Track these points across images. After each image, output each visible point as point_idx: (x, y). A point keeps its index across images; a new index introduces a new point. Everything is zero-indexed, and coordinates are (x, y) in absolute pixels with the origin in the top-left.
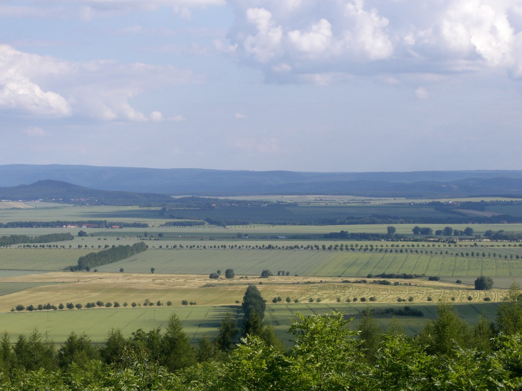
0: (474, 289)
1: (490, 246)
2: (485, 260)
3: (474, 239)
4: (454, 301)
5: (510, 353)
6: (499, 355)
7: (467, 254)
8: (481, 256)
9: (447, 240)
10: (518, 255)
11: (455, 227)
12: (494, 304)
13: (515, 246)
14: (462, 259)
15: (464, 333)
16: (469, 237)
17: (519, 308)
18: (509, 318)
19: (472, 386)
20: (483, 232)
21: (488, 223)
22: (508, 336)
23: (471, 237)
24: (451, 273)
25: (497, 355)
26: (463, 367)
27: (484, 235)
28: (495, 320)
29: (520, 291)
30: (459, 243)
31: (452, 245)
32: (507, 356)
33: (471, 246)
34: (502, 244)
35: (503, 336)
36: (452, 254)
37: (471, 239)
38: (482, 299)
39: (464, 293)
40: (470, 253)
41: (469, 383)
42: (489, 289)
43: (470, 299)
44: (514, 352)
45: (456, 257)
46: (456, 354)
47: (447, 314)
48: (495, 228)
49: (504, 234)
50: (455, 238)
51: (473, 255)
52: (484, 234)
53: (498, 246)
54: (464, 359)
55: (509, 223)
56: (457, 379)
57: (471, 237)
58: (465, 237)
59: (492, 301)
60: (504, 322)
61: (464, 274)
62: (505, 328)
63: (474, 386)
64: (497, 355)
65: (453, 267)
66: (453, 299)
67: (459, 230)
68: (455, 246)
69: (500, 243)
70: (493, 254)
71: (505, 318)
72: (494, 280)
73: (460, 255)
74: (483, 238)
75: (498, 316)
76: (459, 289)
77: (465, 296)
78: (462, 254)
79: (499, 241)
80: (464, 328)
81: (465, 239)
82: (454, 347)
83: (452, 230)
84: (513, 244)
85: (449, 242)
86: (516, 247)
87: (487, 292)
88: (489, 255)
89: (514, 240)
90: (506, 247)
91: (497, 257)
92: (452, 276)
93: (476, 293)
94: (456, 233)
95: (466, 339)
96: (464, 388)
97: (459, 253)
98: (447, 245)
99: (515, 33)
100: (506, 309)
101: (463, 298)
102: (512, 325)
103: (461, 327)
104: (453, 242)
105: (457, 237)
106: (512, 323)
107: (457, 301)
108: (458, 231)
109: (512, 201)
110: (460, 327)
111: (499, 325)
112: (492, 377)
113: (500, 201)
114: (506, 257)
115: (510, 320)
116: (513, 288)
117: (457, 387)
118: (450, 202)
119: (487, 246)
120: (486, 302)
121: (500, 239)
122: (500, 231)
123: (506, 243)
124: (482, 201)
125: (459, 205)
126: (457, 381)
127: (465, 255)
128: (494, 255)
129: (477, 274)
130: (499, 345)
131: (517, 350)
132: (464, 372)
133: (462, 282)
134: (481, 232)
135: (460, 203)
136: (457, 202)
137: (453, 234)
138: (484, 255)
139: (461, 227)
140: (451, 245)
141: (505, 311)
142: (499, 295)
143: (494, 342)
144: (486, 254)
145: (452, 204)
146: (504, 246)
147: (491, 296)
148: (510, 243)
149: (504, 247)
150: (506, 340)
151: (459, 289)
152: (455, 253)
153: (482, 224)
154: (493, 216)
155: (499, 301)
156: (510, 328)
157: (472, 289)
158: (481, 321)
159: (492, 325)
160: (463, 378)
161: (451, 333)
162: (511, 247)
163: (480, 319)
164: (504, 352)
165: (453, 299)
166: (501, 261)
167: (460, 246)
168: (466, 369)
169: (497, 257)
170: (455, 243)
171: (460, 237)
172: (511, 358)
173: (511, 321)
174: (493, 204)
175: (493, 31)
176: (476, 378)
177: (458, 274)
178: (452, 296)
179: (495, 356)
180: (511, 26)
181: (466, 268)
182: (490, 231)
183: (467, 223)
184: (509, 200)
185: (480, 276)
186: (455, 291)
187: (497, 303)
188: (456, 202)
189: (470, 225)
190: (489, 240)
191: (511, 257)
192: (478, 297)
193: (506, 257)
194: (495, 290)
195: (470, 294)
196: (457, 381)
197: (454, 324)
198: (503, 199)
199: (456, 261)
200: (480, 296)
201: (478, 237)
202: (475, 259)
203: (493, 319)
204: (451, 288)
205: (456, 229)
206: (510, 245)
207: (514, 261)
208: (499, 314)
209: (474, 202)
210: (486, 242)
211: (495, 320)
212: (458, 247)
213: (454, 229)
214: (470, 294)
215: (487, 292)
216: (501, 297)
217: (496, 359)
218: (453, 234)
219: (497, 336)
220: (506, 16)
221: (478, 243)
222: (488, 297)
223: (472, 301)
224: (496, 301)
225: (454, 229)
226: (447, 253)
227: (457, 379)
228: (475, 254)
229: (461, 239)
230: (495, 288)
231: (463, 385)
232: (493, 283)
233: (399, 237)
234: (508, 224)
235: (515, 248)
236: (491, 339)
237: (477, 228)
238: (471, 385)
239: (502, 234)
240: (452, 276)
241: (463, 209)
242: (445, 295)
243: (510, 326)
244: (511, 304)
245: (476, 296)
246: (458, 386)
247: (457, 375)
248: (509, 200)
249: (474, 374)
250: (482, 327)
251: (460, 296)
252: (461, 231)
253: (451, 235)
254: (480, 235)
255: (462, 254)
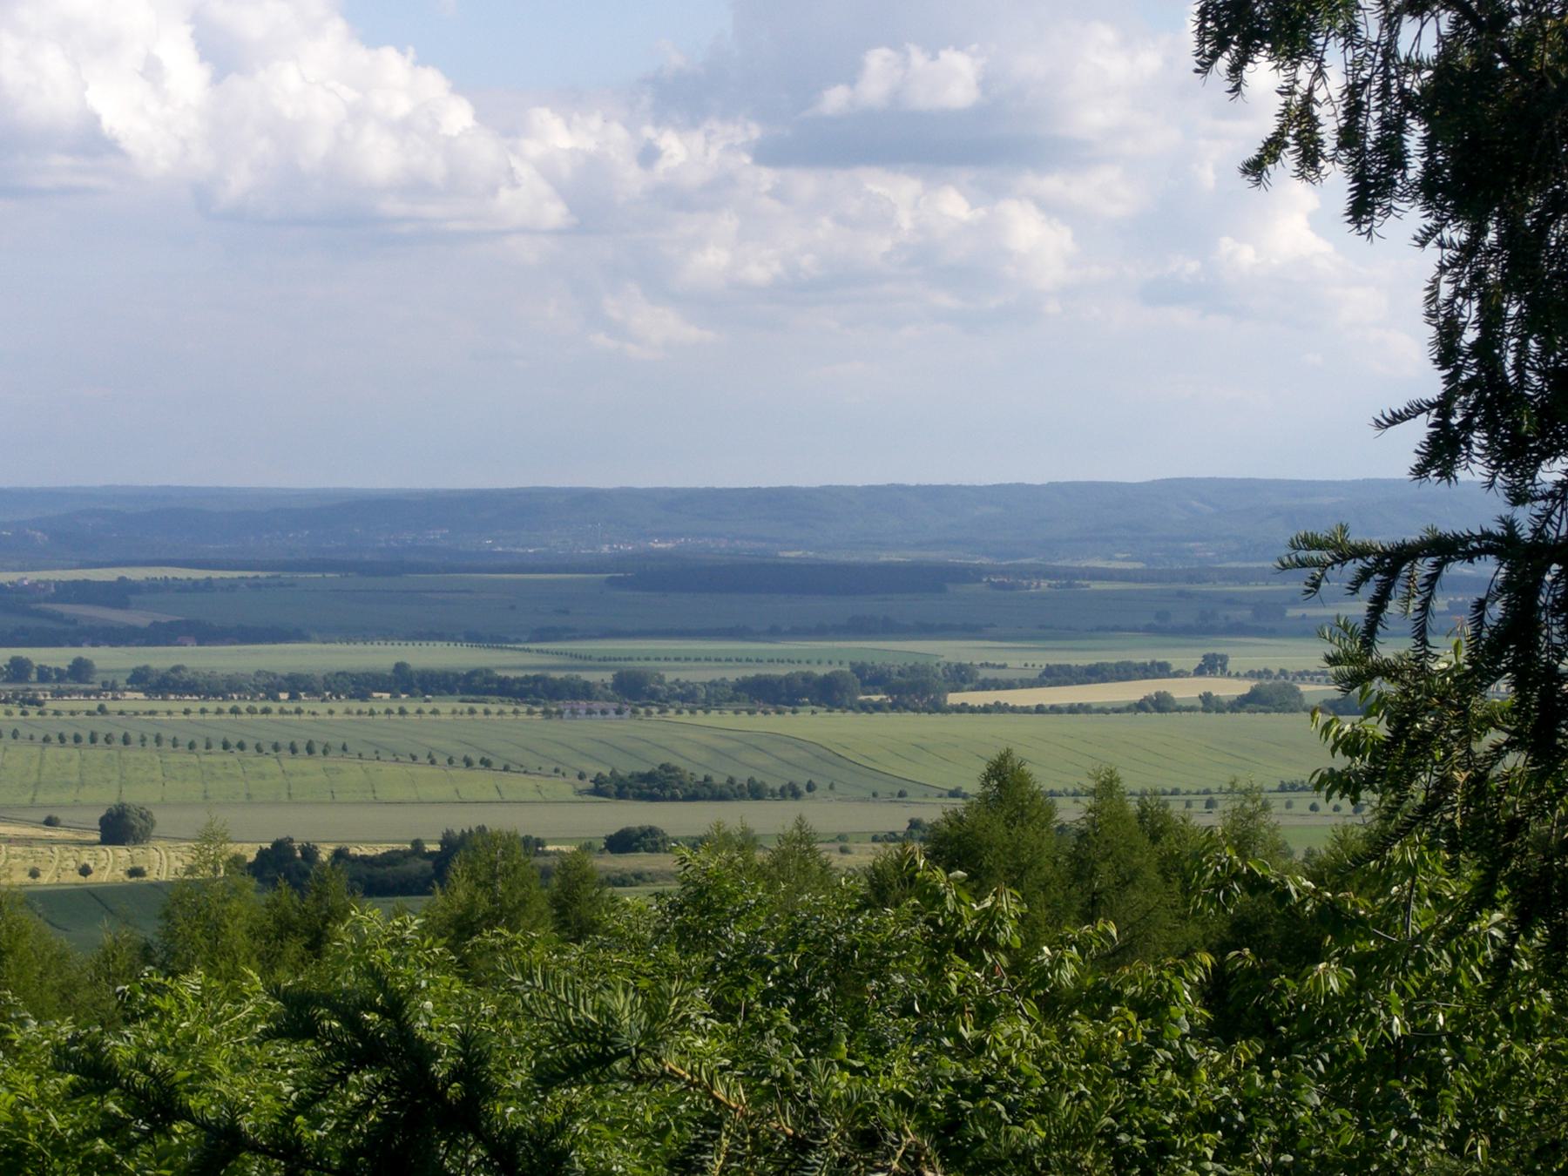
0: (99, 844)
1: (145, 713)
2: (132, 754)
3: (97, 693)
4: (38, 880)
5: (172, 1030)
6: (140, 1035)
7: (77, 739)
8: (118, 744)
9: (15, 697)
10: (229, 740)
11: (40, 656)
12: (157, 886)
13: (219, 712)
14: (63, 753)
15: (60, 973)
16: (82, 686)
17: (226, 896)
18: (196, 927)
19: (56, 1133)
20: (126, 671)
21: (137, 645)
22: (170, 979)
23: (89, 687)
24: (29, 796)
25: (132, 1037)
26: (29, 1073)
27: (129, 682)
28: (155, 933)
29: (229, 845)
30: (51, 705)
31: (33, 712)
32: (162, 1038)
33: (89, 713)
34: (181, 706)
35: (155, 979)
36: (31, 738)
37: (87, 694)
38: (122, 873)
39: (67, 854)
40: (85, 736)
41: (47, 1121)
42: (142, 842)
43: (85, 871)
44: (183, 1025)
45: (43, 748)
46: (11, 1037)
47: (10, 920)
48: (160, 658)
49: (187, 676)
50: (40, 690)
51: (93, 740)
52: (128, 676)
53: (169, 713)
54: (34, 1049)
55: (199, 644)
56: (13, 1111)
57: (89, 687)
58: (72, 686)
59: (152, 876)
60: (181, 938)
61: (68, 797)
62: (184, 956)
63: (62, 1130)
64: (132, 1037)
65: (34, 777)
66: (34, 874)
67: (52, 665)
68: (41, 713)
69: (175, 704)
70: (153, 738)
71: (185, 926)
72: (158, 815)
73: (55, 740)
74: (126, 690)
75: (162, 923)
76: (52, 842)
77: (72, 864)
78: (62, 739)
79: (172, 697)
80: (61, 958)
81: (70, 692)
82: (13, 1015)
83: (32, 666)
84: (212, 705)
85: (24, 702)
86: (223, 717)
87: (137, 851)
88: (143, 740)
89: (216, 695)
90: (192, 717)
91: (167, 746)
92: (33, 805)
93: (103, 855)
94: (44, 675)
95: (65, 991)
96: (31, 1136)
97: (51, 735)
98: (17, 711)
99: (217, 79)
100: (186, 901)
101: (64, 870)
102: (205, 949)
103: (52, 958)
104: (34, 702)
105: (47, 686)
106: (203, 941)
107: (46, 879)
108: (50, 669)
109: (209, 579)
110: (48, 955)
111: (165, 949)
112: (116, 1103)
113: (175, 579)
114: (192, 746)
115: (198, 932)
116: (209, 837)
117: (12, 1136)
118: (26, 583)
119: (136, 713)
120: (134, 880)
121: (175, 693)
122: (176, 669)
123: (193, 703)
124: (122, 579)
125: (53, 590)
126: (10, 1118)
127: (70, 742)
128: (158, 740)
129: (107, 798)
130: (142, 1005)
131: (193, 1019)
132: (32, 1088)
133: (62, 823)
134: (118, 671)
135: (57, 584)
136: (47, 583)
137: (34, 676)
138: (126, 740)
139: (58, 657)
140: (29, 711)
141: (183, 907)
142: (173, 859)
143: (129, 998)
144: (134, 736)
145: (34, 586)
146: (187, 712)
147: (149, 861)
148: (205, 705)
149: (185, 717)
150: (160, 990)
151: (52, 842)
152: (39, 736)
153: (122, 649)
154: (155, 624)
155: (172, 877)
156: (198, 957)
157: (91, 844)
158: (107, 939)
159: (145, 949)
160: (31, 1107)
161: (20, 975)
162: (207, 717)
163: (105, 933)
164: (155, 1027)
165: (34, 874)
166: (175, 758)
167: (57, 713)
168: (38, 1082)
169: (167, 746)
170: (40, 704)
171: (56, 686)
172: (173, 1044)
173: (201, 935)
174: (153, 587)
175: (152, 70)
176: (69, 1105)
177: (51, 798)
178: (31, 863)
179: (128, 1039)
180: (203, 58)
181: (76, 779)
182: (146, 668)
183: (75, 644)
184: (199, 574)
185: (115, 802)
186: (40, 850)
187: (167, 883)
188: (42, 582)
189: (86, 652)
190: (141, 695)
191: (208, 747)
192: (109, 868)
193: (192, 746)
194: (160, 844)
195: (86, 857)
196: (10, 1118)
197: (31, 948)
198: (183, 574)
199: (42, 759)
200: (115, 862)
201: (110, 687)
202: (99, 753)
203: (150, 931)
204: (28, 841)
205: (43, 663)
206: (203, 711)
207: (217, 758)
208: (168, 915)
209: (100, 582)
210: (134, 700)
211: (155, 933)
212: (50, 715)
213: (36, 663)
214: (86, 857)
215: (136, 851)
216: (179, 864)
217: (129, 1049)
218: (34, 676)
219: (137, 980)
220: (189, 29)
221: (111, 706)
222: (138, 865)
223: (91, 878)
224: (163, 877)
225: (36, 663)
226: (15, 735)
227: (13, 1111)
228: (101, 738)
229: (58, 694)
230: (159, 838)
231: (27, 1130)
232: (153, 824)
233: (286, 713)
234: (199, 648)
235: (218, 717)
236: (119, 989)
237: (106, 658)
238: (53, 1128)
239: (181, 677)
240: (33, 805)
241: (63, 602)
242: (12, 861)
243: (197, 952)
244: (202, 886)
245: (103, 864)
246: (15, 1133)
247: (12, 1098)
248: (199, 574)
249: (63, 1094)
250: (114, 955)
251: (56, 863)
252: (58, 670)
253: (27, 682)
254: (114, 682)
255: (62, 739)
